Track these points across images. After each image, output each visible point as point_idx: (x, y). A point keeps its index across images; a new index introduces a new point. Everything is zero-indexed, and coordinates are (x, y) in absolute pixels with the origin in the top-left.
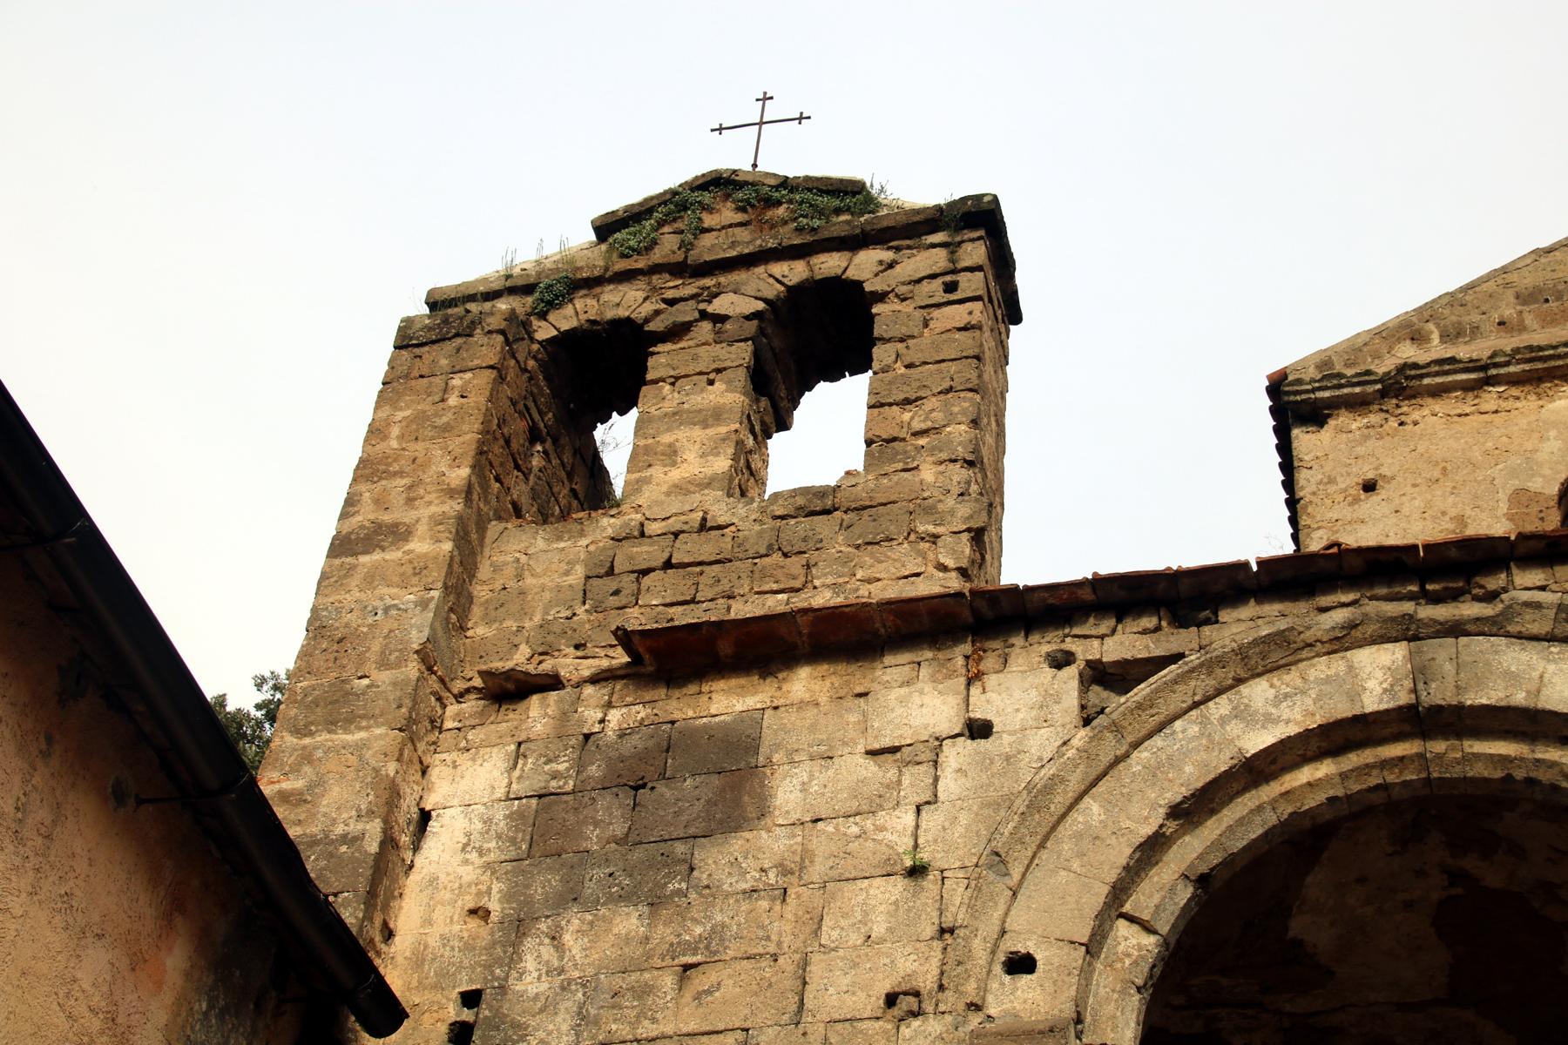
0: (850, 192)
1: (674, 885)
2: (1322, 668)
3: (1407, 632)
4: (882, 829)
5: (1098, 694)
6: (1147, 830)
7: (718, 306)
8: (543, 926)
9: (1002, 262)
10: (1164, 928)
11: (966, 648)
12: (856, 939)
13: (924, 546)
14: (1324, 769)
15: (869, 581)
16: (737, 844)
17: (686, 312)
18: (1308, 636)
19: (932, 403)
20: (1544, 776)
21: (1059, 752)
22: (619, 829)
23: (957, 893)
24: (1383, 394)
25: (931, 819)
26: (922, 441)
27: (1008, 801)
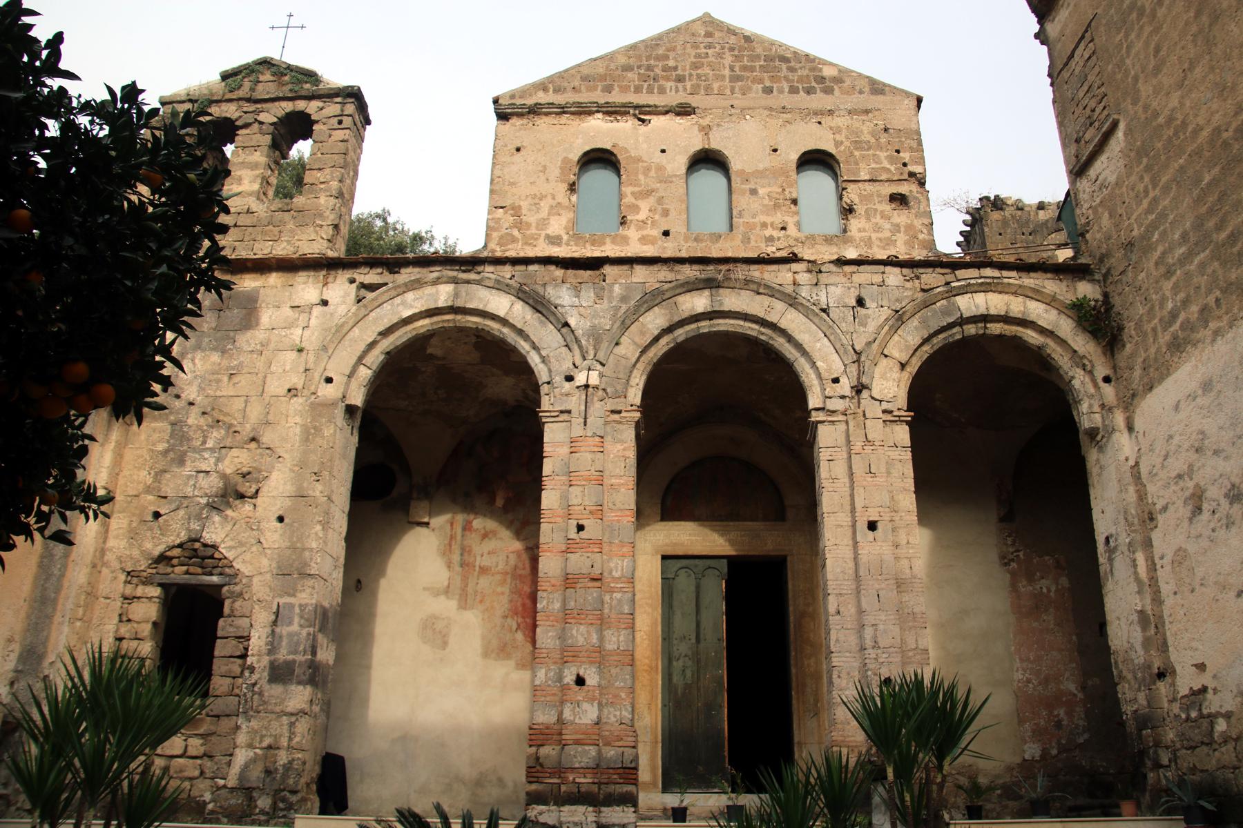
0: (311, 76)
1: (229, 347)
2: (429, 290)
3: (455, 281)
4: (292, 334)
5: (363, 292)
6: (371, 340)
7: (262, 117)
8: (190, 356)
9: (362, 107)
10: (374, 368)
11: (324, 272)
12: (281, 370)
13: (318, 229)
14: (426, 322)
15: (299, 240)
16: (249, 334)
17: (249, 118)
18: (426, 280)
19: (328, 171)
20: (486, 328)
21: (347, 314)
22: (214, 325)
23: (312, 358)
24: (529, 113)
25: (307, 333)
26: (322, 186)
27: (330, 329)
